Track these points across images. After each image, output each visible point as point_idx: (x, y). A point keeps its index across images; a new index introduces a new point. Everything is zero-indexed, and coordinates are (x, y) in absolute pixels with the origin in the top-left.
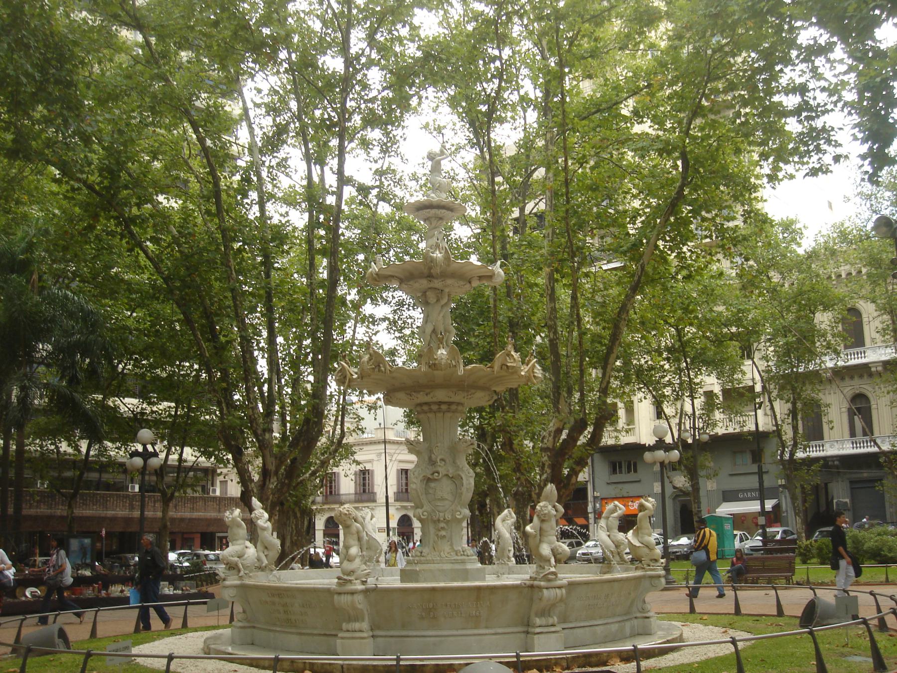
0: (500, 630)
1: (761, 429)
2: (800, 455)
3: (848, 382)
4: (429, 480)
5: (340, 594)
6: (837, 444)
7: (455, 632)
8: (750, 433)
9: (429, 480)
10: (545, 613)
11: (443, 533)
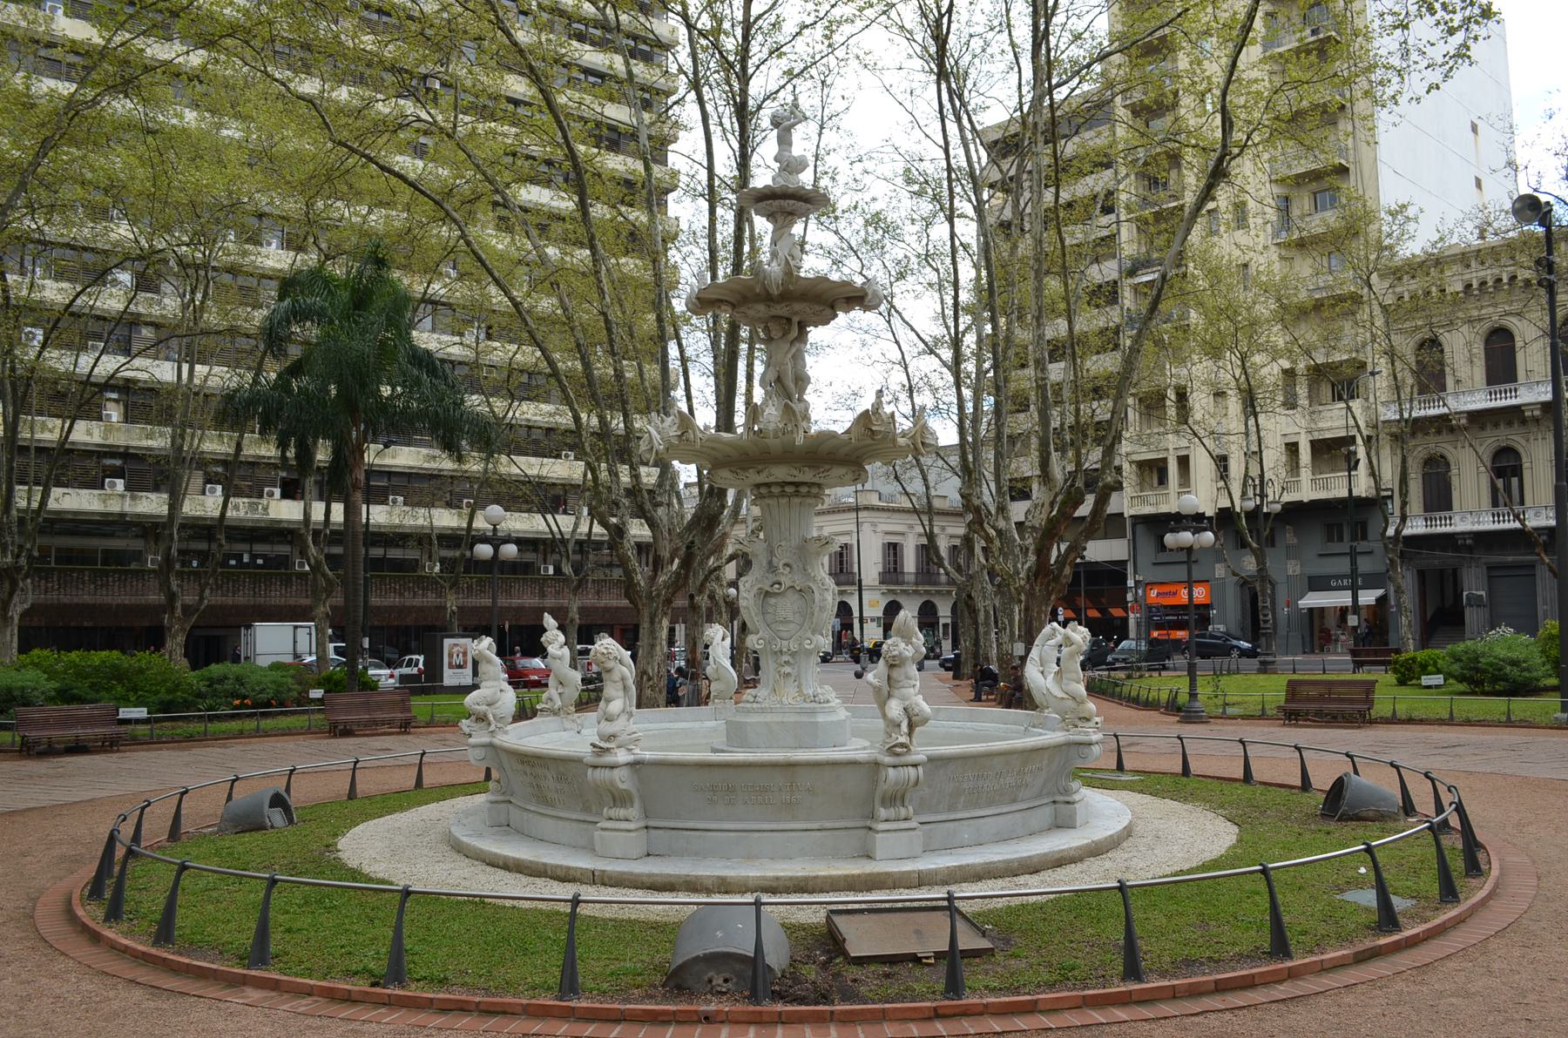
5: (596, 767)
6: (1472, 514)
10: (895, 798)
11: (787, 669)
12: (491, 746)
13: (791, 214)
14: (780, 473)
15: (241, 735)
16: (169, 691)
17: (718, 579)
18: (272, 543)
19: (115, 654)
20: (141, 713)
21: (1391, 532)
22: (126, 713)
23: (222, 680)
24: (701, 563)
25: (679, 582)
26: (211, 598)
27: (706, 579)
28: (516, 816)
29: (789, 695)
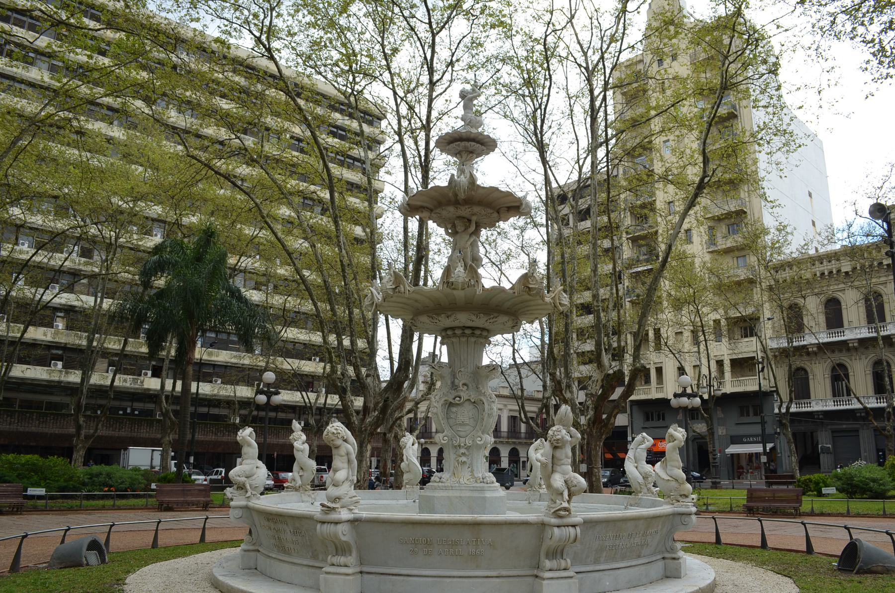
0: (504, 573)
2: (793, 409)
4: (451, 404)
5: (323, 523)
6: (822, 401)
9: (451, 404)
10: (556, 553)
11: (464, 459)
12: (247, 508)
13: (471, 152)
14: (463, 319)
15: (103, 508)
16: (65, 481)
17: (400, 426)
18: (145, 402)
19: (36, 456)
20: (41, 491)
21: (776, 411)
22: (32, 491)
23: (98, 475)
24: (391, 414)
25: (377, 423)
26: (103, 432)
27: (394, 423)
28: (262, 561)
29: (465, 477)
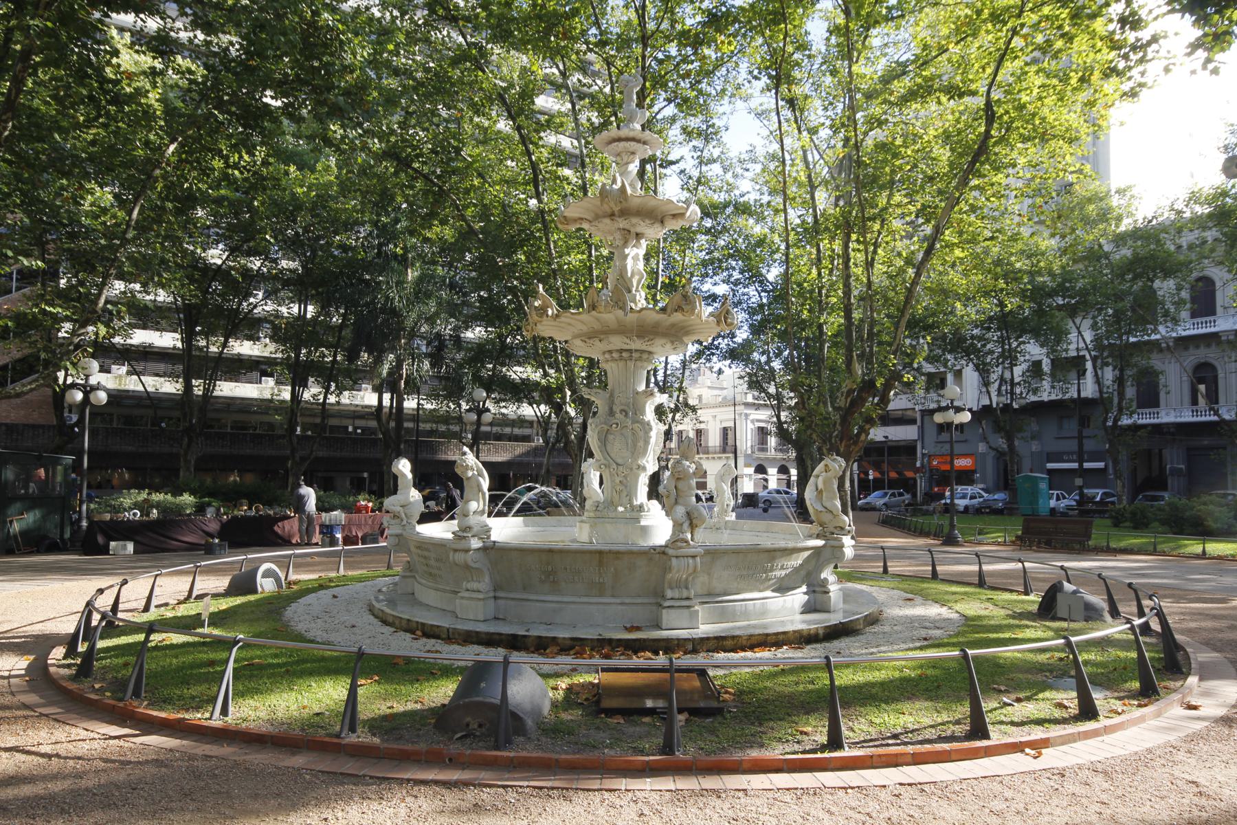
0: (627, 601)
1: (1083, 395)
2: (1125, 421)
3: (1192, 350)
5: (456, 551)
7: (578, 600)
8: (1072, 400)
21: (1110, 423)
